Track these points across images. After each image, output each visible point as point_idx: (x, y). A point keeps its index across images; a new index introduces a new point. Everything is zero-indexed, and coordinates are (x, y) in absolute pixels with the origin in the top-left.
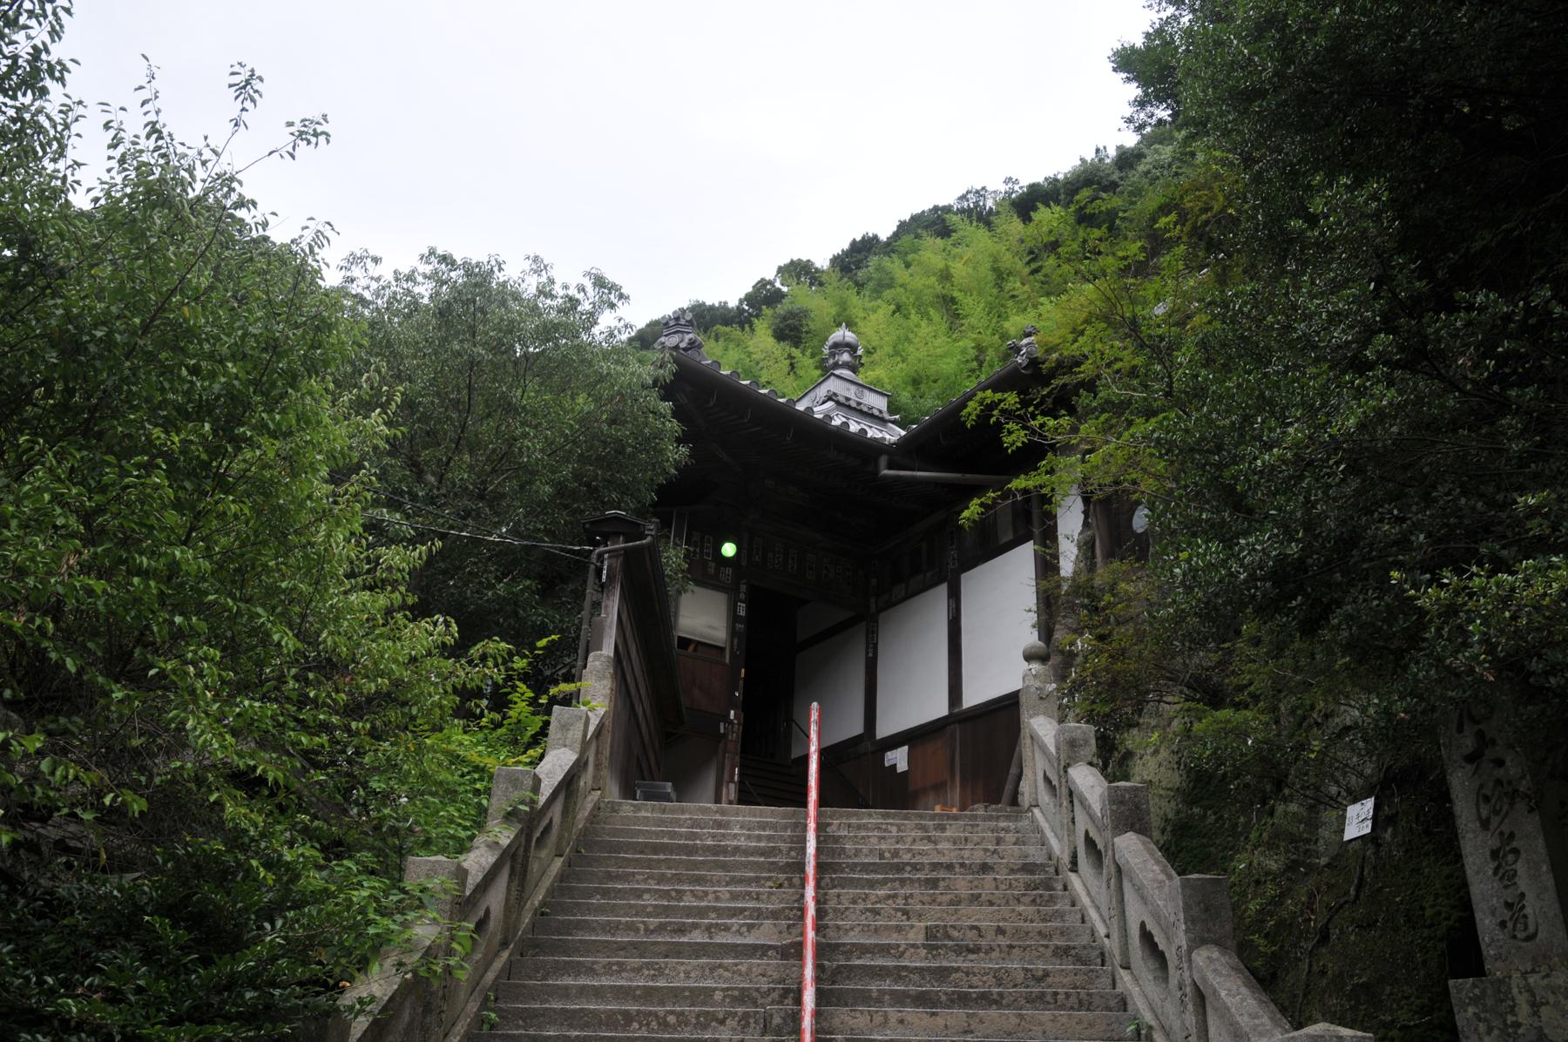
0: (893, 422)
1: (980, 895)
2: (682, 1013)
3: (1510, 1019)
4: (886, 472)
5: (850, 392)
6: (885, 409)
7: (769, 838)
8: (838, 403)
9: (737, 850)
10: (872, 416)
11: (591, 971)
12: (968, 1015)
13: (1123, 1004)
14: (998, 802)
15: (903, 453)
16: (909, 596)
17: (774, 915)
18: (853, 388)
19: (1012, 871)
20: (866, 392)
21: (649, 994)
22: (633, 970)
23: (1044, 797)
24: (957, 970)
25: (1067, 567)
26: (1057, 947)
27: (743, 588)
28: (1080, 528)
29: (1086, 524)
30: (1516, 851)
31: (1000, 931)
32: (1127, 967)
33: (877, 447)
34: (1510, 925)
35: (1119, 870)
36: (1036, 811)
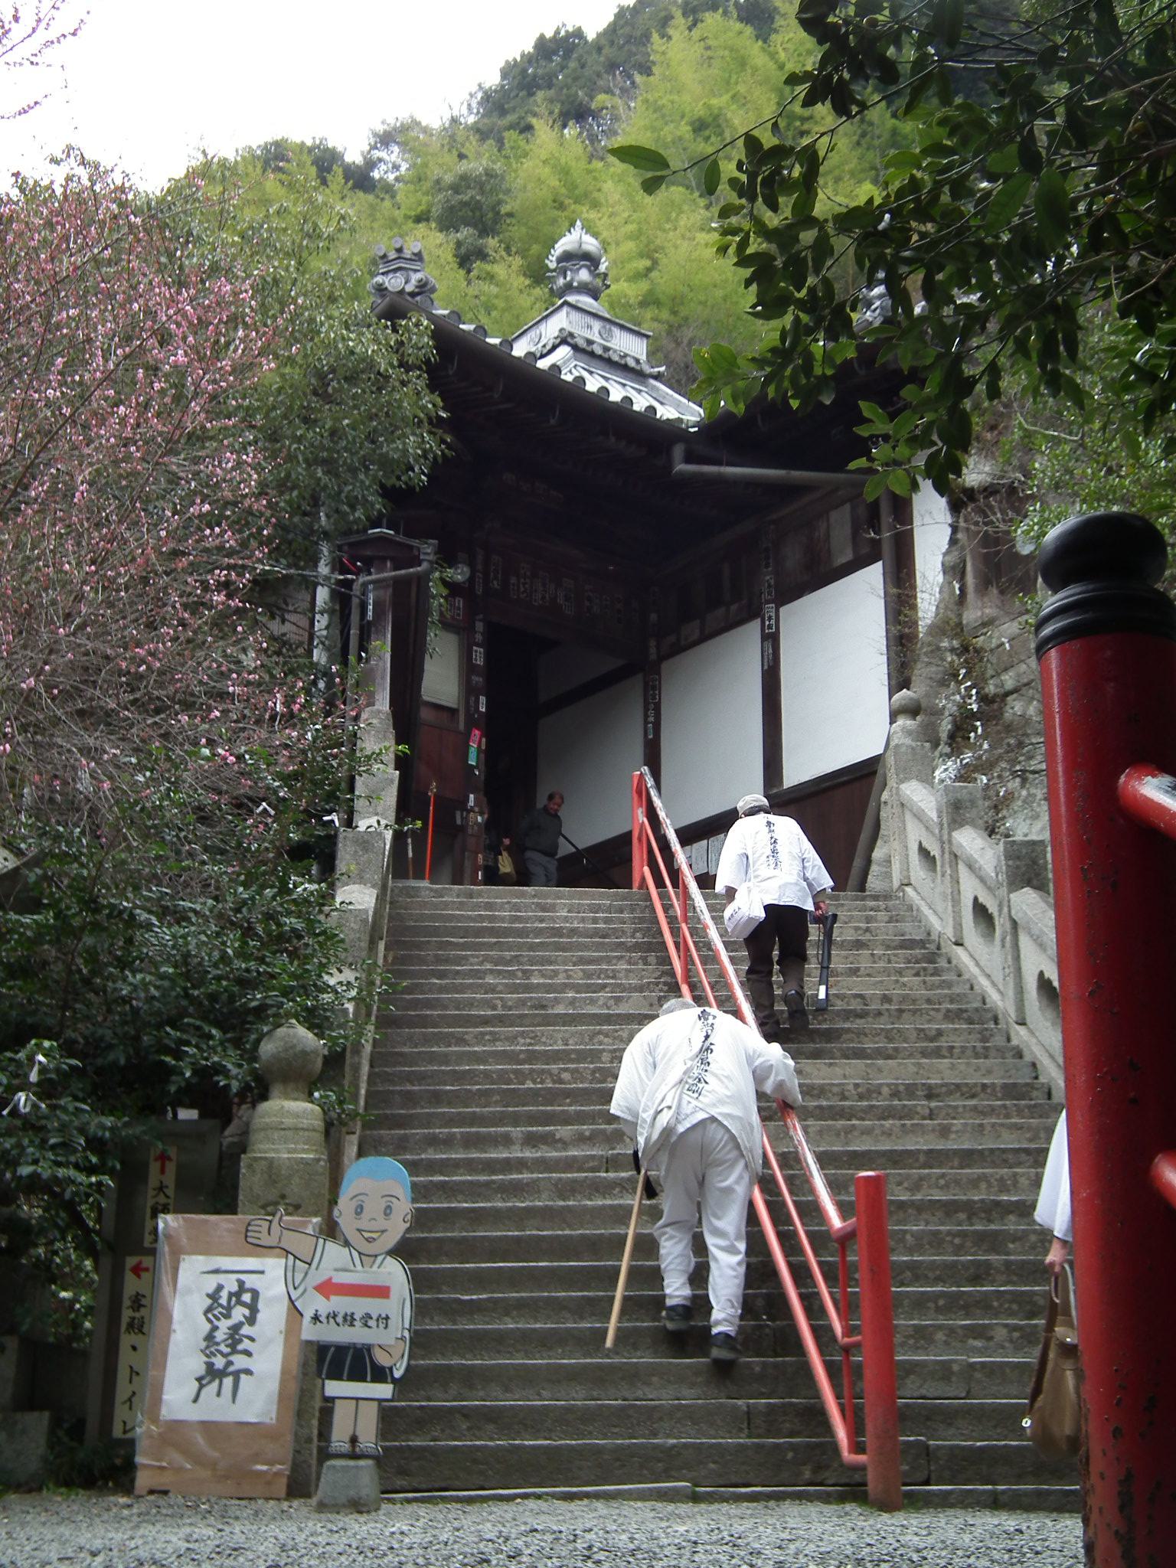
0: (657, 377)
1: (858, 969)
2: (576, 1070)
4: (681, 467)
5: (594, 332)
6: (643, 358)
7: (607, 921)
8: (575, 348)
9: (573, 932)
10: (632, 370)
11: (461, 1040)
12: (867, 1065)
13: (1019, 1054)
15: (719, 436)
16: (704, 638)
17: (640, 989)
18: (597, 325)
19: (888, 948)
20: (616, 331)
21: (532, 1057)
22: (507, 1039)
23: (918, 871)
24: (848, 1030)
25: (928, 602)
26: (949, 1010)
27: (480, 626)
28: (945, 546)
29: (953, 541)
31: (886, 999)
32: (1022, 1023)
33: (672, 432)
35: (1015, 924)
36: (908, 889)
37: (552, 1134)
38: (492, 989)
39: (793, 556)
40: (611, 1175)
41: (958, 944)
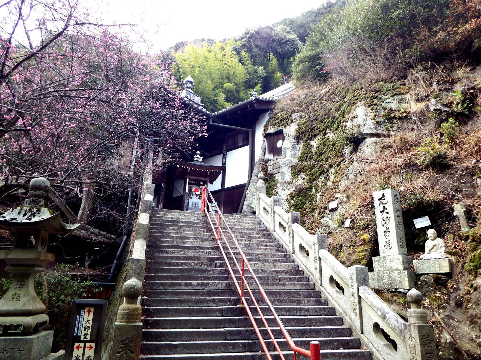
0: (202, 106)
3: (385, 264)
6: (200, 102)
11: (167, 252)
14: (237, 212)
25: (258, 155)
30: (389, 231)
34: (386, 246)
37: (161, 240)
38: (173, 237)
39: (230, 142)
40: (208, 298)
41: (274, 231)
